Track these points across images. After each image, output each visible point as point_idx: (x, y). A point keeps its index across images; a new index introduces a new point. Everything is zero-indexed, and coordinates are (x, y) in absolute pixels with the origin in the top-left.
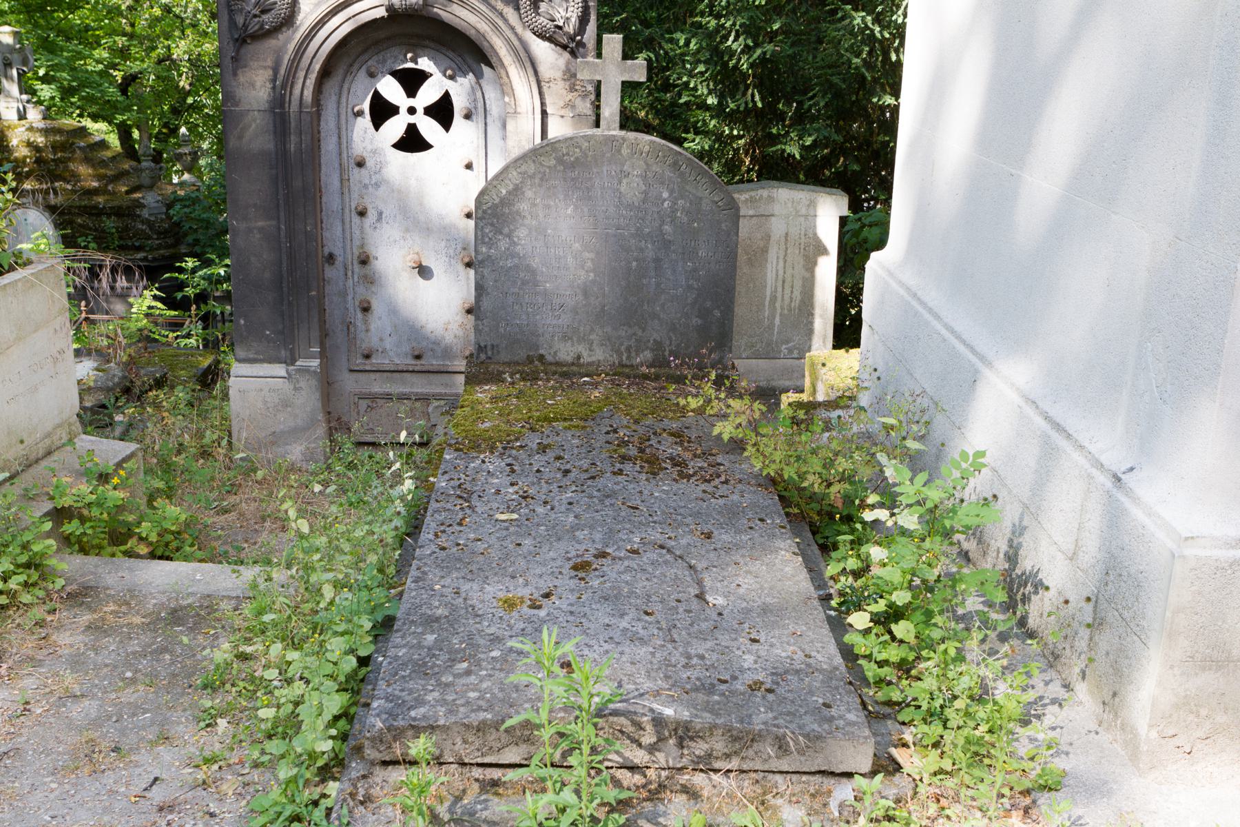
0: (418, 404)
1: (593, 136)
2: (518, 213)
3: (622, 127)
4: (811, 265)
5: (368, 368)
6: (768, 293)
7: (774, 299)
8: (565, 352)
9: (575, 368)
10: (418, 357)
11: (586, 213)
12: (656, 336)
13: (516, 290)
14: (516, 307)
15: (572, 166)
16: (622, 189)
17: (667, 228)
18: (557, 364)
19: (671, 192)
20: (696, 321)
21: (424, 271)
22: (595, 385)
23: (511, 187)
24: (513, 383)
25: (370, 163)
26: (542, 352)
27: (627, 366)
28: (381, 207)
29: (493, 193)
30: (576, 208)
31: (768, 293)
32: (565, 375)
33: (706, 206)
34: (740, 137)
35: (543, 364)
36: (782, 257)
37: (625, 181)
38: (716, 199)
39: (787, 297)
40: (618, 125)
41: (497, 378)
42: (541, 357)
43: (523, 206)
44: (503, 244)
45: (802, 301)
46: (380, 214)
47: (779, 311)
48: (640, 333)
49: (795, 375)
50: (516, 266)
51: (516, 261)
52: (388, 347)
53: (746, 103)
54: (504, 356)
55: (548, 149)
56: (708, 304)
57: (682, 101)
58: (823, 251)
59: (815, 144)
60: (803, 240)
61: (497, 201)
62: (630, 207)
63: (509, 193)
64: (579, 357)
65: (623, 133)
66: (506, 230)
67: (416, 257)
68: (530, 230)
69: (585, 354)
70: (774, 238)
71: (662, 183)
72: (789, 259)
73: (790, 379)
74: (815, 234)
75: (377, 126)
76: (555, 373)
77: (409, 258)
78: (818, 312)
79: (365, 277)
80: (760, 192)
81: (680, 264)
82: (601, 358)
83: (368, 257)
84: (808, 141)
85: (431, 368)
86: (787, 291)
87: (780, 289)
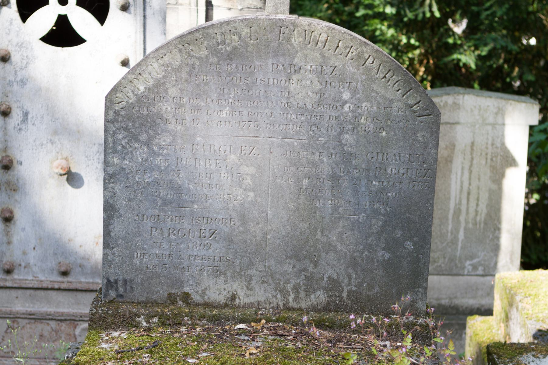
0: (64, 326)
1: (256, 20)
2: (159, 115)
3: (292, 11)
4: (498, 177)
5: (9, 284)
6: (452, 205)
7: (457, 212)
8: (217, 291)
9: (228, 311)
10: (65, 274)
11: (245, 117)
12: (331, 272)
13: (156, 212)
14: (155, 233)
15: (230, 56)
16: (292, 88)
17: (347, 137)
18: (207, 305)
19: (354, 92)
20: (382, 255)
21: (72, 178)
22: (253, 335)
23: (151, 82)
24: (148, 330)
25: (15, 58)
26: (187, 289)
27: (294, 309)
28: (28, 106)
29: (128, 90)
30: (233, 111)
31: (452, 205)
32: (215, 319)
33: (398, 110)
34: (414, 48)
35: (188, 304)
36: (467, 166)
37: (295, 77)
38: (411, 102)
39: (472, 210)
40: (287, 7)
41: (128, 322)
42: (186, 297)
43: (166, 107)
44: (141, 153)
45: (489, 215)
46: (26, 114)
47: (463, 225)
48: (311, 268)
49: (480, 293)
50: (156, 182)
51: (156, 175)
52: (32, 261)
53: (424, 13)
54: (138, 295)
55: (198, 35)
56: (398, 234)
57: (358, 14)
58: (511, 162)
59: (491, 55)
60: (490, 150)
61: (133, 100)
62: (302, 110)
63: (149, 90)
64: (233, 297)
65: (294, 17)
66: (144, 137)
67: (64, 163)
68: (174, 136)
69: (241, 293)
70: (459, 147)
71: (342, 81)
72: (475, 170)
73: (474, 297)
74: (503, 144)
75: (24, 17)
76: (202, 317)
77: (56, 163)
78: (505, 226)
79: (8, 183)
80: (445, 98)
81: (363, 183)
82: (262, 299)
83: (11, 162)
84: (484, 51)
85: (79, 286)
86: (473, 204)
87: (464, 202)
